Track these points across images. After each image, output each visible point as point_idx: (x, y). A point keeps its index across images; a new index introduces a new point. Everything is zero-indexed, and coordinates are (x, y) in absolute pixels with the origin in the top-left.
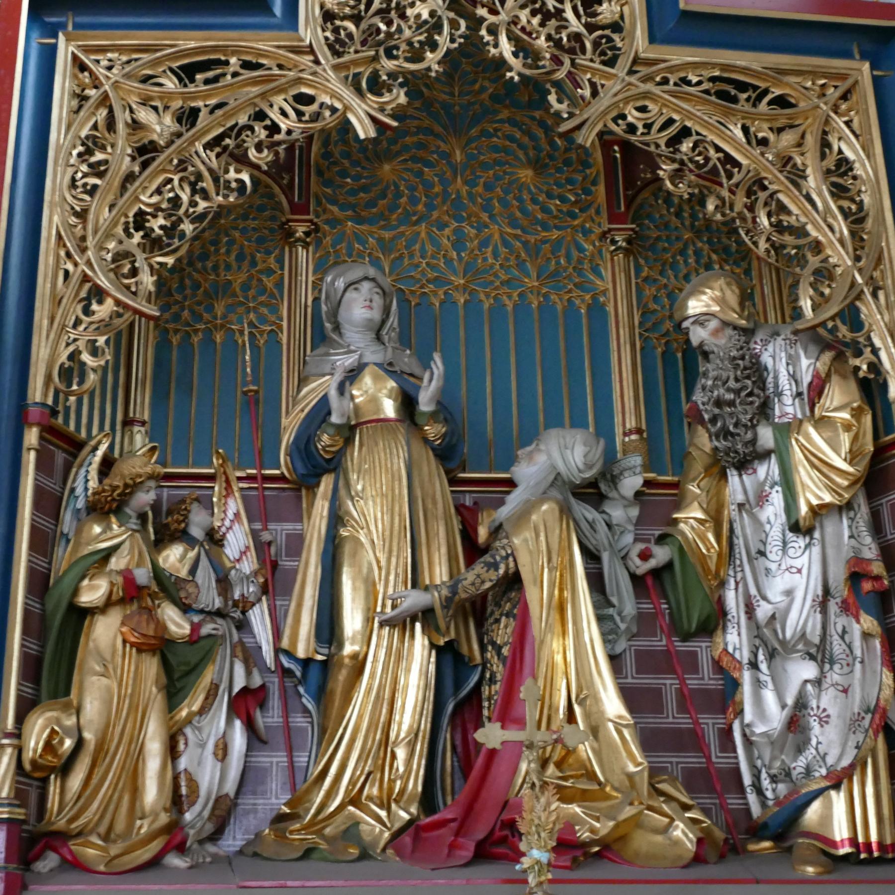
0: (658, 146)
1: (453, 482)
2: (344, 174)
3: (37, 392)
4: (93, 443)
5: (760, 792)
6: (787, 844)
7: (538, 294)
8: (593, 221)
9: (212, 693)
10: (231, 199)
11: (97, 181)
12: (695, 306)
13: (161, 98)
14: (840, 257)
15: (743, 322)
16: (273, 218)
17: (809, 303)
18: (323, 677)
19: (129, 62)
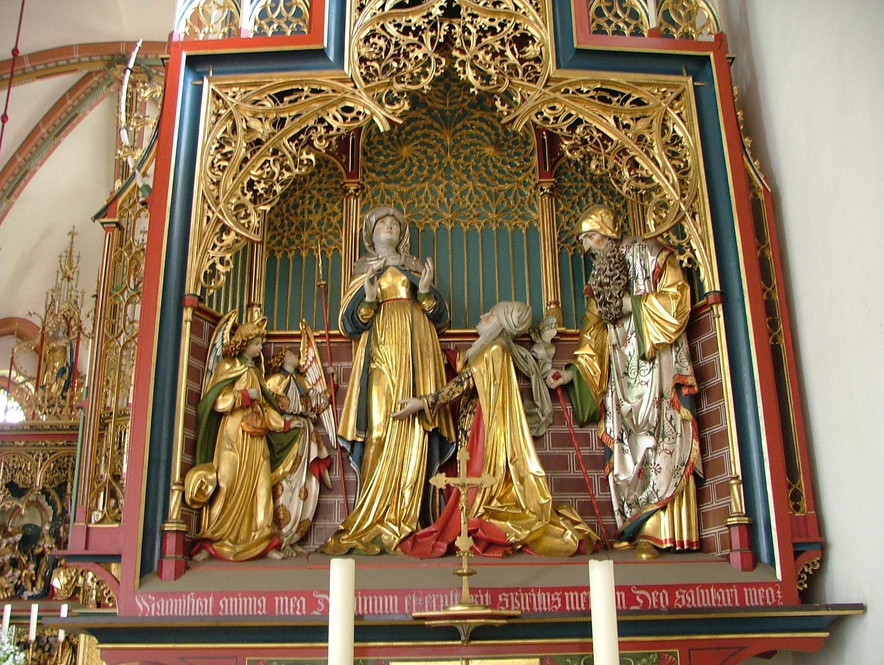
0: (562, 130)
1: (441, 335)
2: (379, 154)
3: (190, 287)
4: (226, 317)
5: (623, 514)
6: (634, 543)
7: (497, 222)
8: (530, 177)
9: (298, 460)
10: (303, 170)
11: (226, 163)
12: (586, 226)
13: (263, 113)
14: (672, 194)
15: (615, 235)
16: (337, 182)
17: (653, 222)
18: (359, 451)
19: (245, 93)
